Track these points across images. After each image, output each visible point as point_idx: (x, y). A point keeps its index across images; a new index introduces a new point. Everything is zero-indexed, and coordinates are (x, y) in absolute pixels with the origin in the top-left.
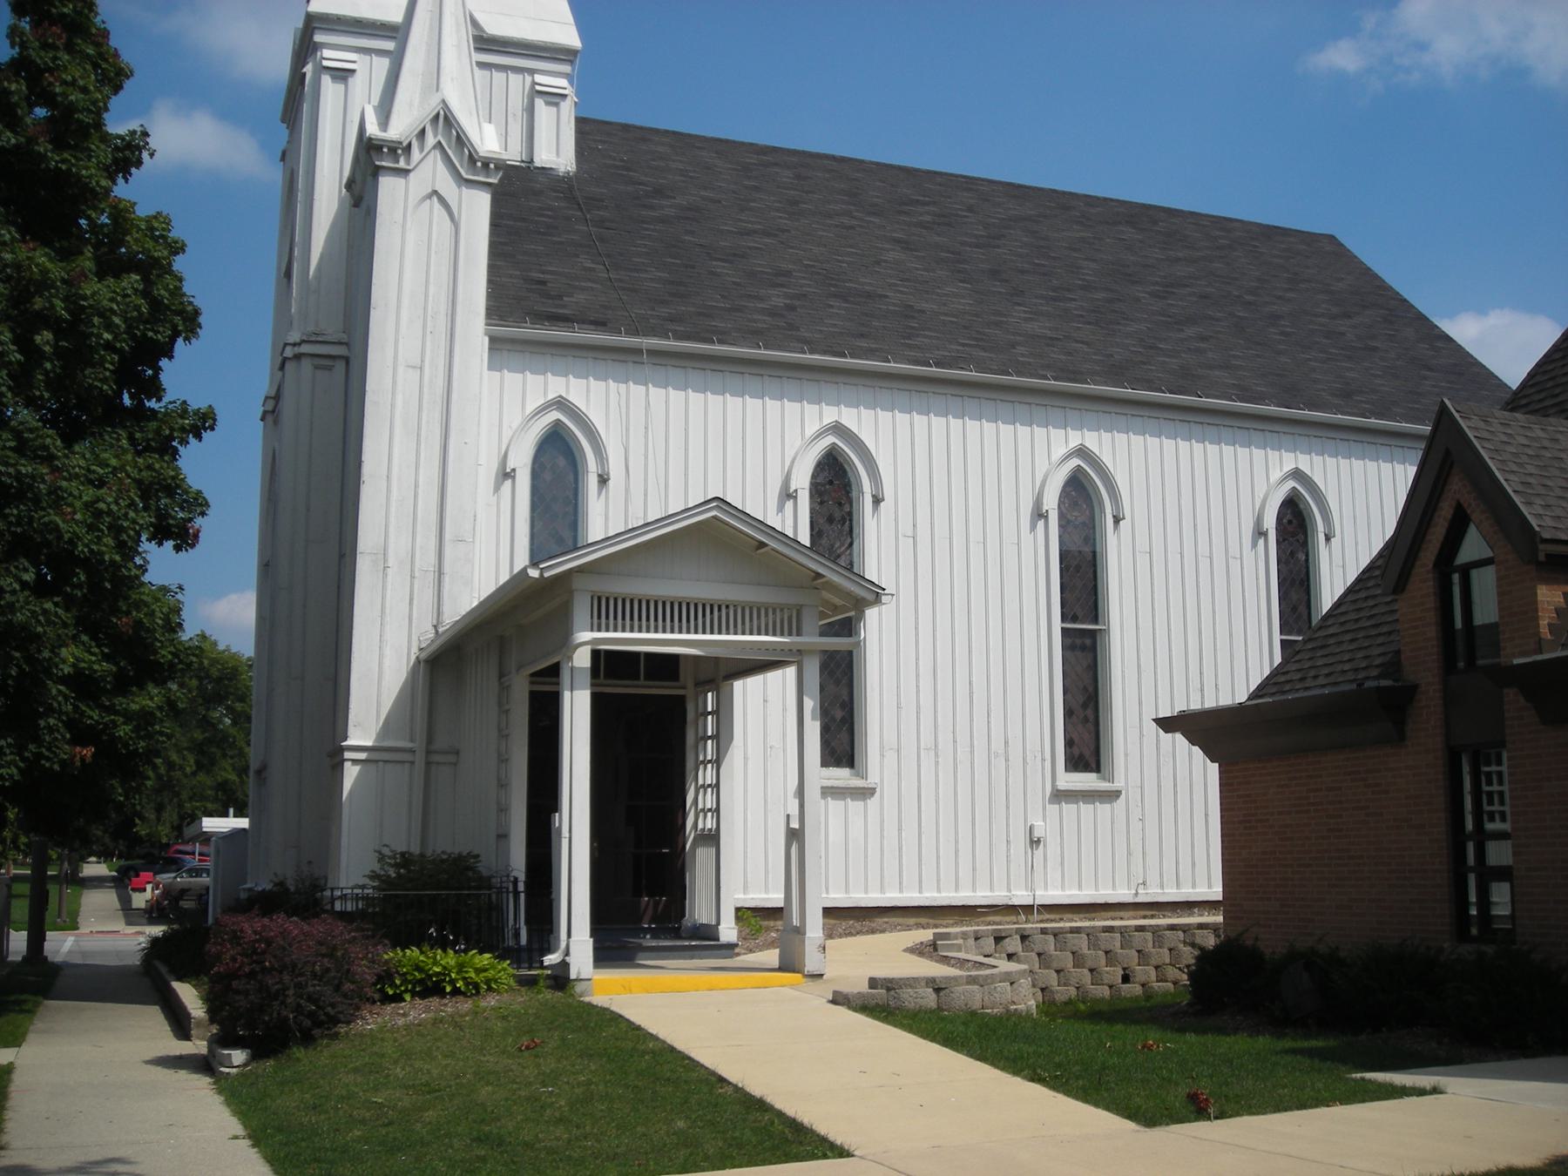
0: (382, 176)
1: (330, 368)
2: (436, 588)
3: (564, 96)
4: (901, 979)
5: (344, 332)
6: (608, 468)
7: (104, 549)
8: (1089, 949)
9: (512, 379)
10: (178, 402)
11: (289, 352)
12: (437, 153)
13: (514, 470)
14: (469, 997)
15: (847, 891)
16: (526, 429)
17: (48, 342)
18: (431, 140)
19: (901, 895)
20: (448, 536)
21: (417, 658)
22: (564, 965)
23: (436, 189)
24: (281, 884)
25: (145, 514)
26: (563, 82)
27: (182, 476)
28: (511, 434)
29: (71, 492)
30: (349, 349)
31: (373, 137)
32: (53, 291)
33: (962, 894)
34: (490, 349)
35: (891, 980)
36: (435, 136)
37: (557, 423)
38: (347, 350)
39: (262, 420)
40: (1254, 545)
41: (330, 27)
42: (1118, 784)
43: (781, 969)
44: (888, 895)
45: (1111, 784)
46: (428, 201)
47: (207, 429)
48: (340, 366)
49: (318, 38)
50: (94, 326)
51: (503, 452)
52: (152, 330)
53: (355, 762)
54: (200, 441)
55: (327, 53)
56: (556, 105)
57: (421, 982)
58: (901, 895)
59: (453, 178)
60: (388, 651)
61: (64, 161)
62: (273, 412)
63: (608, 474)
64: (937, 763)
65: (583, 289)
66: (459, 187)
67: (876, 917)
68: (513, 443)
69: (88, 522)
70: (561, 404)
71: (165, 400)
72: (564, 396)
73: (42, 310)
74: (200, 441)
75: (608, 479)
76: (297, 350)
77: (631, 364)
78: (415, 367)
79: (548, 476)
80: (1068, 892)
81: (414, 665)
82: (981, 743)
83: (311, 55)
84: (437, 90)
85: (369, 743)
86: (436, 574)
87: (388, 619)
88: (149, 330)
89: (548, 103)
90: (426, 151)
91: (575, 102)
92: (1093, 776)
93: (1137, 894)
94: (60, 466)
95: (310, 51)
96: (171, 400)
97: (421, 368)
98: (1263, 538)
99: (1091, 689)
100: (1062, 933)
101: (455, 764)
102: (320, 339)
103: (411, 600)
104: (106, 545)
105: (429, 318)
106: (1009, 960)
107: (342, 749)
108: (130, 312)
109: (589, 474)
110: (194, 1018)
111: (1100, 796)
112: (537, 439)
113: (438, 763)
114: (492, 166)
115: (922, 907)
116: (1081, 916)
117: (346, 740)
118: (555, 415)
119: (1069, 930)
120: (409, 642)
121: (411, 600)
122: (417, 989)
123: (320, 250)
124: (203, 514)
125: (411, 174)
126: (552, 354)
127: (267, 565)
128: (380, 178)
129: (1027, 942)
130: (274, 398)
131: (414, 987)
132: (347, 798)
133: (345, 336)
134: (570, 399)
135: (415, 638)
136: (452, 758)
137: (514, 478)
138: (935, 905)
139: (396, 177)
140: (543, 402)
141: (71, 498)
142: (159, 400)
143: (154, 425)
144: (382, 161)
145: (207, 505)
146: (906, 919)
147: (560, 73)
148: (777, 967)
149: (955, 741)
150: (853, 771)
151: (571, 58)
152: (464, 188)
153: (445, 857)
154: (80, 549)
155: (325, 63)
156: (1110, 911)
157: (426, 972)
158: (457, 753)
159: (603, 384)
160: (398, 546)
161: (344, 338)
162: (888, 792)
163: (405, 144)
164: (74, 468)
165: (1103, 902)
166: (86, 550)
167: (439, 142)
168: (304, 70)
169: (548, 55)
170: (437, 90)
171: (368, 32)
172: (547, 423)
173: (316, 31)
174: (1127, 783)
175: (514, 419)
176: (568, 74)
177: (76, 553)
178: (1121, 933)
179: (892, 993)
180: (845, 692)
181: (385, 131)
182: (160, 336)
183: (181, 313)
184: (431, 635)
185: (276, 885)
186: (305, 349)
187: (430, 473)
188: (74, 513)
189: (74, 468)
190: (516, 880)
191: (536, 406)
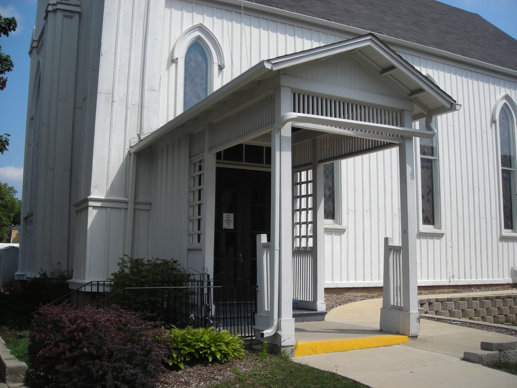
1: (71, 17)
2: (139, 115)
4: (507, 344)
6: (224, 62)
8: (455, 309)
9: (177, 14)
11: (50, 8)
13: (177, 59)
14: (223, 364)
15: (333, 280)
16: (183, 39)
19: (356, 282)
20: (146, 86)
21: (129, 151)
22: (276, 336)
24: (45, 275)
30: (81, 9)
33: (366, 281)
35: (501, 345)
37: (198, 38)
40: (491, 126)
42: (443, 231)
43: (381, 331)
44: (350, 282)
45: (440, 230)
47: (11, 30)
48: (76, 17)
53: (94, 207)
57: (190, 354)
58: (356, 282)
60: (113, 147)
62: (37, 47)
63: (224, 65)
64: (371, 218)
67: (345, 292)
68: (178, 43)
70: (201, 28)
72: (202, 23)
74: (8, 36)
76: (54, 7)
77: (234, 13)
79: (193, 64)
80: (423, 281)
81: (127, 155)
82: (389, 209)
85: (103, 197)
86: (140, 107)
87: (113, 129)
92: (431, 227)
93: (450, 281)
98: (494, 124)
99: (431, 186)
100: (444, 301)
101: (149, 210)
103: (126, 120)
106: (470, 319)
107: (87, 200)
109: (214, 64)
110: (8, 368)
111: (436, 236)
112: (188, 45)
113: (140, 210)
115: (365, 287)
116: (428, 291)
117: (90, 195)
118: (197, 33)
119: (446, 299)
120: (125, 143)
121: (126, 120)
122: (187, 360)
124: (9, 70)
127: (32, 119)
129: (431, 306)
131: (185, 358)
132: (90, 227)
133: (79, 2)
134: (205, 25)
135: (128, 141)
136: (147, 207)
137: (177, 63)
138: (370, 286)
140: (191, 26)
146: (357, 293)
148: (377, 327)
149: (378, 208)
150: (334, 221)
153: (159, 262)
156: (439, 289)
157: (193, 347)
158: (150, 204)
160: (120, 91)
162: (350, 231)
165: (437, 285)
172: (194, 36)
174: (446, 230)
175: (177, 33)
178: (467, 301)
179: (502, 353)
180: (330, 183)
184: (136, 140)
185: (41, 275)
186: (59, 6)
187: (137, 54)
190: (208, 276)
191: (187, 29)
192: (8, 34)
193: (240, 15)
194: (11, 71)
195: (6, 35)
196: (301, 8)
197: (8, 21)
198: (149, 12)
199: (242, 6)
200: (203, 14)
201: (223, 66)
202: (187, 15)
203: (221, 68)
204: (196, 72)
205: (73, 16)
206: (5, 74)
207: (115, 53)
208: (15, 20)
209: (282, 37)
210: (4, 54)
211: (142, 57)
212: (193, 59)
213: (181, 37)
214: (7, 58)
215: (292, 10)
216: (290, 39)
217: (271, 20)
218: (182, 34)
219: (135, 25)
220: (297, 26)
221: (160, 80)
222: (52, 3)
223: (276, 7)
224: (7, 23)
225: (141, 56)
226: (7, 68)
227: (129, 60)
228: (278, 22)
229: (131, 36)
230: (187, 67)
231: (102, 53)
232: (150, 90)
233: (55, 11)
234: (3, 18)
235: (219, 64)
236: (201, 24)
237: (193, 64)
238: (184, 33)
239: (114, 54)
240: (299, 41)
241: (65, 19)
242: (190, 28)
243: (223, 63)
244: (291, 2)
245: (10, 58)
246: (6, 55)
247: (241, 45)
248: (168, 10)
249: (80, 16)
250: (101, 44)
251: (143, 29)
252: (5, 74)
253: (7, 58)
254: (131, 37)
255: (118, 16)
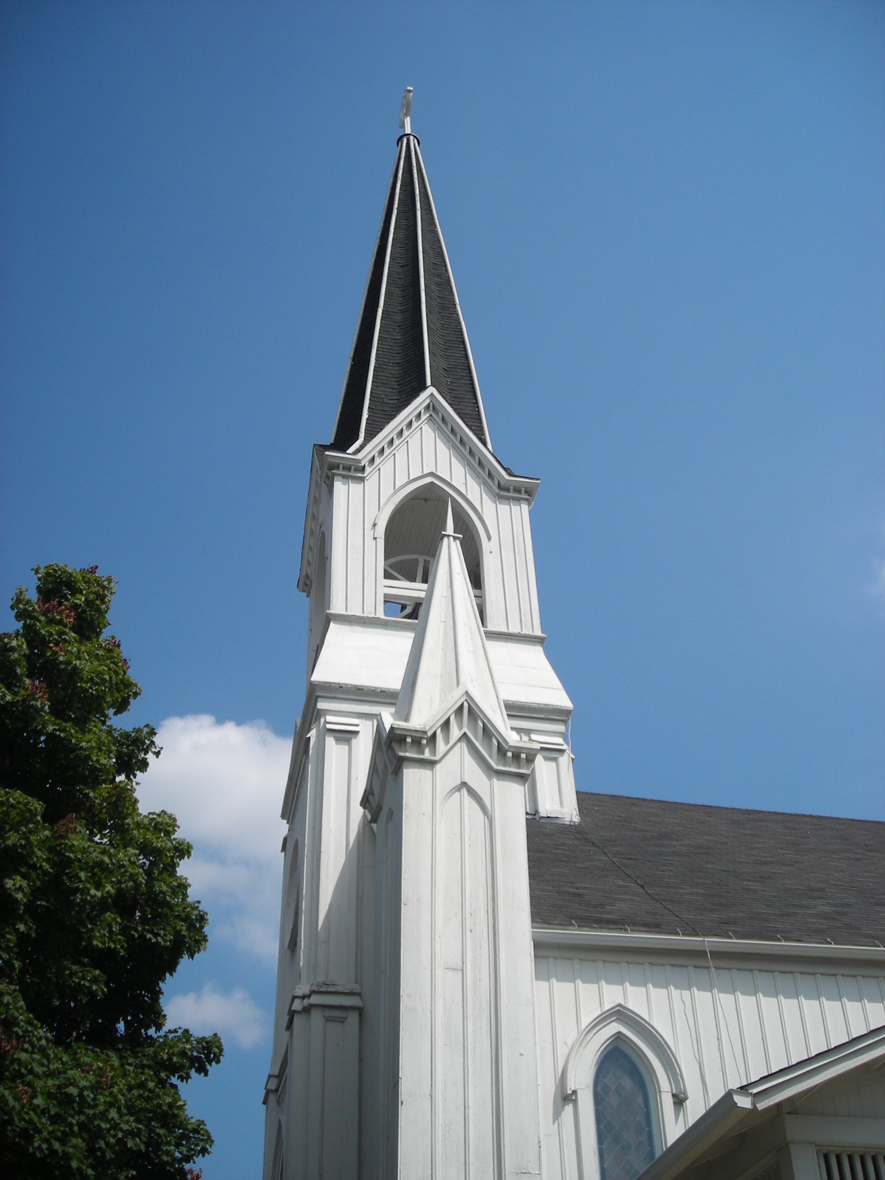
0: (406, 768)
1: (342, 1020)
3: (562, 751)
5: (356, 983)
7: (71, 1150)
9: (563, 989)
10: (180, 1032)
11: (297, 1005)
12: (464, 745)
17: (21, 889)
18: (455, 732)
23: (466, 781)
25: (132, 1119)
26: (560, 740)
27: (181, 1103)
28: (567, 1051)
29: (32, 1068)
31: (395, 726)
32: (31, 826)
34: (535, 957)
36: (460, 728)
37: (618, 1037)
38: (360, 1002)
39: (264, 1103)
41: (332, 695)
46: (457, 794)
48: (353, 1019)
49: (321, 705)
50: (81, 881)
51: (560, 1072)
52: (152, 932)
54: (206, 1074)
55: (329, 718)
56: (555, 760)
59: (484, 773)
61: (63, 730)
62: (277, 1090)
63: (685, 1093)
65: (623, 900)
66: (490, 779)
69: (52, 1113)
70: (620, 1013)
71: (165, 1029)
72: (623, 1004)
73: (14, 845)
74: (206, 1074)
75: (686, 1098)
76: (306, 1002)
77: (691, 969)
78: (455, 969)
83: (315, 722)
84: (458, 685)
88: (148, 931)
89: (546, 759)
90: (452, 742)
91: (572, 758)
94: (21, 1034)
95: (314, 719)
96: (173, 1029)
97: (463, 970)
102: (331, 989)
104: (74, 1147)
105: (468, 916)
108: (125, 882)
114: (523, 756)
118: (615, 1027)
123: (329, 901)
124: (204, 1151)
125: (438, 766)
126: (604, 961)
128: (404, 770)
130: (277, 1077)
133: (357, 986)
134: (630, 1007)
137: (575, 1102)
139: (422, 768)
140: (600, 1013)
141: (30, 1077)
142: (159, 1027)
143: (151, 1051)
144: (405, 751)
145: (209, 1140)
147: (555, 732)
151: (564, 718)
152: (495, 780)
154: (36, 1144)
155: (329, 726)
159: (664, 992)
161: (357, 988)
163: (430, 734)
164: (39, 1039)
166: (44, 1146)
167: (465, 734)
168: (308, 735)
169: (543, 716)
170: (458, 685)
171: (370, 699)
173: (319, 700)
175: (568, 1034)
176: (564, 733)
177: (31, 1150)
181: (407, 720)
182: (160, 939)
183: (187, 919)
186: (315, 999)
188: (33, 1097)
189: (39, 1039)
192: (208, 1071)
193: (705, 971)
194: (209, 1154)
195: (203, 1074)
196: (845, 932)
197: (204, 1044)
198: (500, 995)
199: (706, 952)
200: (621, 983)
201: (684, 1094)
202: (587, 990)
203: (681, 1100)
204: (623, 1119)
205: (346, 1018)
206: (194, 1163)
207: (431, 1097)
208: (219, 1041)
209: (810, 1006)
210: (192, 1118)
211: (492, 1099)
212: (613, 1089)
213: (580, 1040)
214: (199, 1126)
215: (823, 941)
216: (832, 1007)
217: (780, 972)
218: (580, 1032)
219: (470, 1029)
220: (843, 975)
221: (540, 1147)
222: (299, 992)
223: (787, 939)
224: (204, 1048)
225: (490, 1096)
226: (199, 1148)
227: (465, 1108)
228: (795, 972)
229: (464, 1052)
230: (599, 1108)
231: (402, 1100)
232: (517, 1173)
233: (307, 1010)
234: (194, 1037)
235: (674, 1092)
236: (620, 1005)
237: (613, 1100)
238: (585, 1030)
239: (430, 1098)
240: (853, 1008)
241: (331, 1026)
242: (595, 1019)
243: (682, 1088)
244: (819, 921)
245: (205, 1125)
246: (197, 1121)
247: (718, 1040)
248: (544, 985)
249: (361, 1016)
250: (400, 1080)
251: (489, 1034)
252: (194, 1163)
253: (199, 1126)
254: (464, 1056)
255: (432, 1013)
